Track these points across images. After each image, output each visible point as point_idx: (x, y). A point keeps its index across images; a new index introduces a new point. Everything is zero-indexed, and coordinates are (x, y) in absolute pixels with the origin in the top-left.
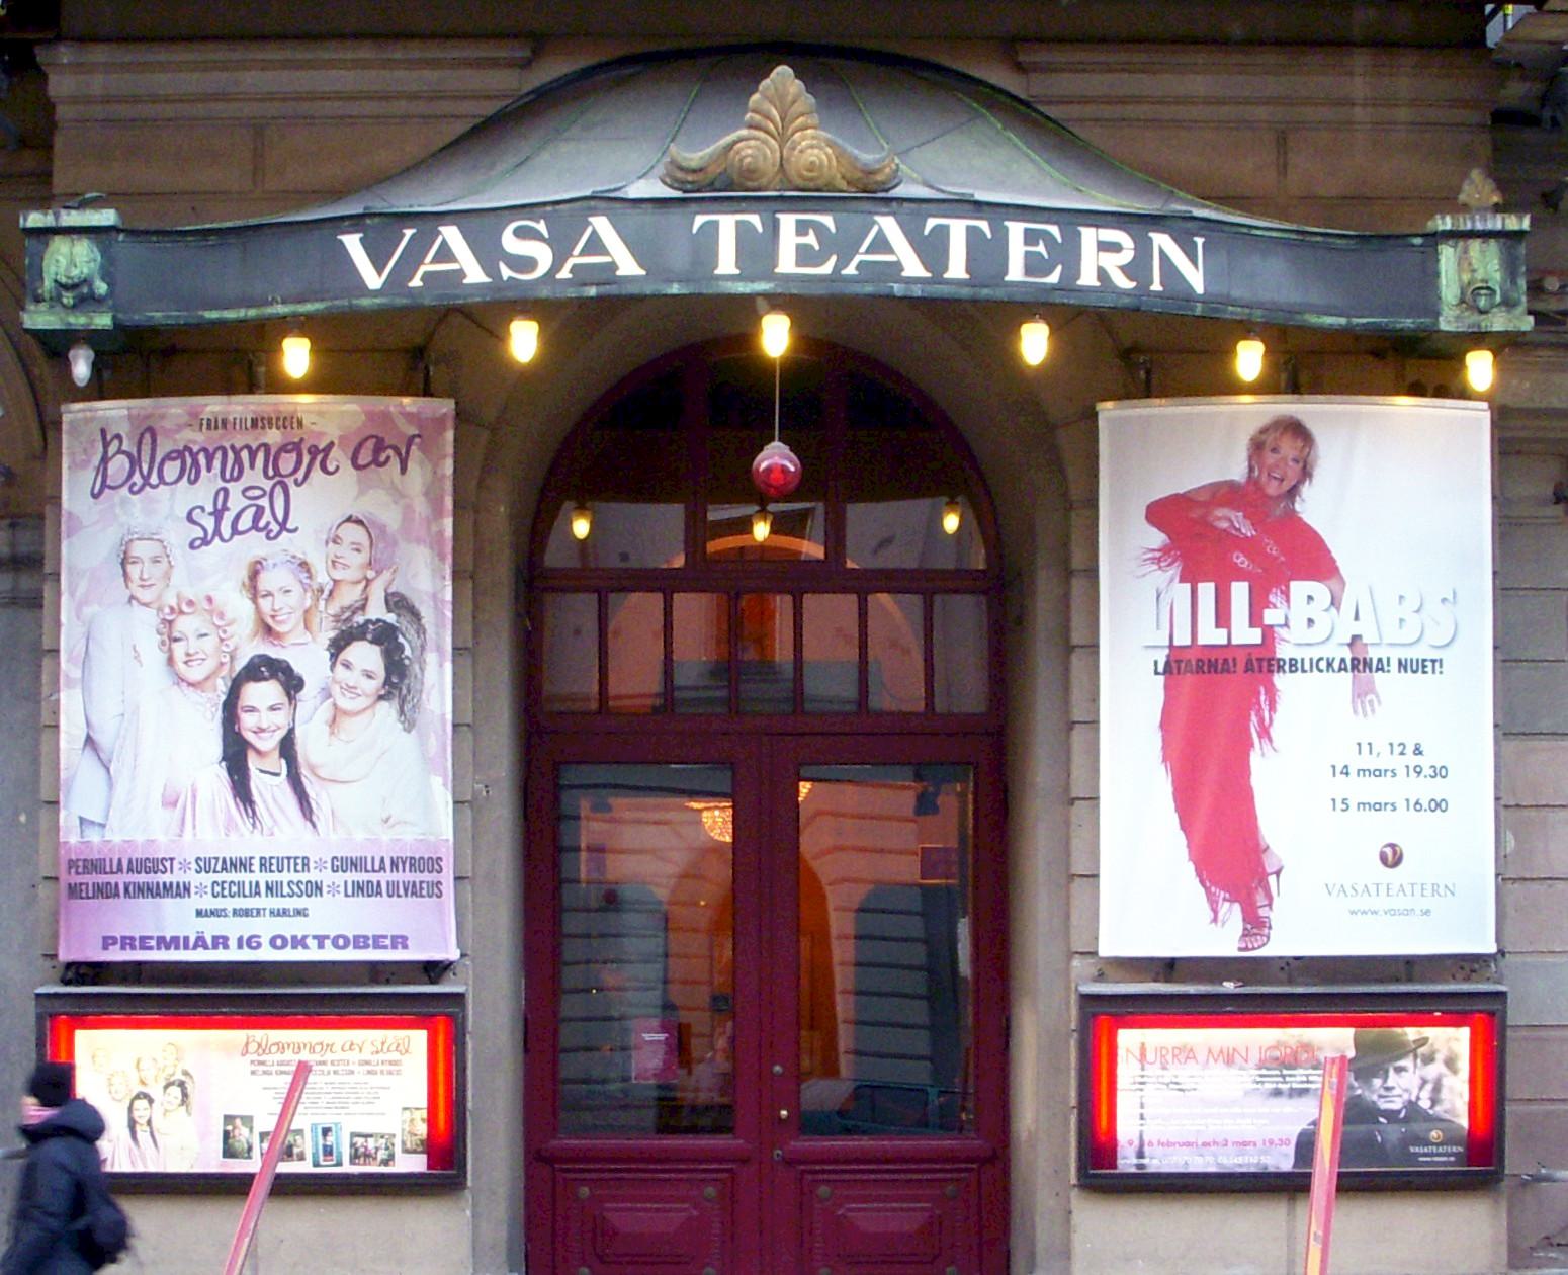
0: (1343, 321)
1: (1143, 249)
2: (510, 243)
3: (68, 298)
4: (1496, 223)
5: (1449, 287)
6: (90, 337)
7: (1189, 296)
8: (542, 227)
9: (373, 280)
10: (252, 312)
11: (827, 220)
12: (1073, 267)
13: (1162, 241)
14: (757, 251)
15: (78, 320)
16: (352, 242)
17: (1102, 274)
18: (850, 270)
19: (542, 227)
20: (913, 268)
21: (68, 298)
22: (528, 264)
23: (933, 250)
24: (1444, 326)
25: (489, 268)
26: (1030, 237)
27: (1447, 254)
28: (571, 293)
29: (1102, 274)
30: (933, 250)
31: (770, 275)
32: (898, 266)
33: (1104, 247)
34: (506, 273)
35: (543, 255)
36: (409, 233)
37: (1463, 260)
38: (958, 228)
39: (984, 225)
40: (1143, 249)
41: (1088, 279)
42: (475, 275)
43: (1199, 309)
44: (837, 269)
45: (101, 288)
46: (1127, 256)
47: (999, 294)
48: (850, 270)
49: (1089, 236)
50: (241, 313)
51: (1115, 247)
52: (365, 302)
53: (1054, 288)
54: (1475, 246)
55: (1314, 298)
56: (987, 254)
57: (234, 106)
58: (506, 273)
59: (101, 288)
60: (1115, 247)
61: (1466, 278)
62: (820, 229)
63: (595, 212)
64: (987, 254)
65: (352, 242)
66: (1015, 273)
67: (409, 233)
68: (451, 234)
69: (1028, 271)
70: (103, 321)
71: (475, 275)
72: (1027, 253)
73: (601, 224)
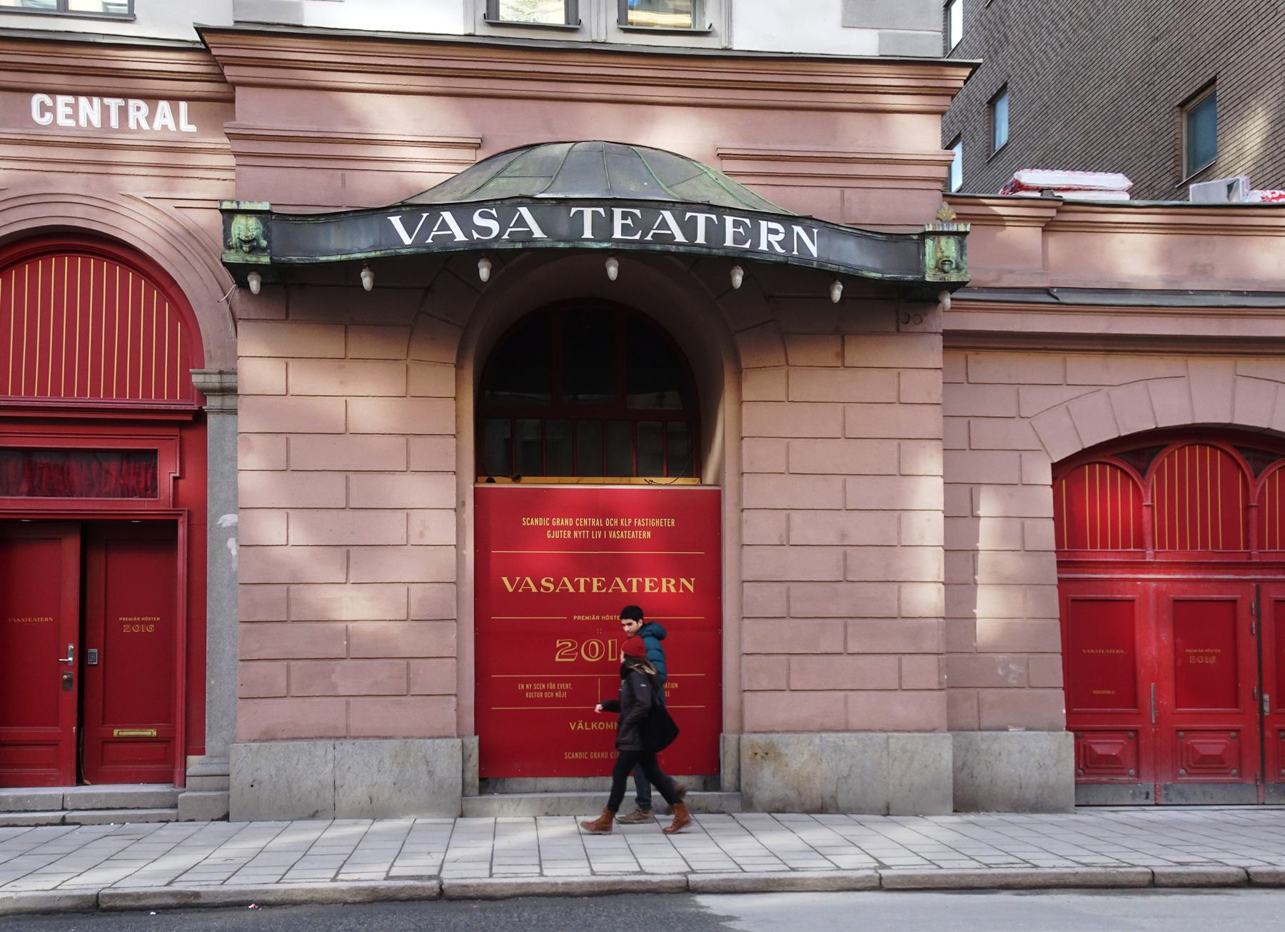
0: (879, 275)
1: (789, 233)
2: (477, 220)
3: (246, 248)
4: (954, 228)
5: (930, 261)
6: (257, 268)
7: (811, 259)
8: (494, 212)
9: (407, 240)
10: (344, 257)
11: (637, 212)
12: (757, 242)
13: (798, 229)
14: (603, 227)
15: (252, 259)
16: (396, 221)
17: (770, 244)
18: (649, 238)
19: (494, 212)
20: (680, 237)
21: (246, 248)
22: (488, 231)
23: (689, 228)
24: (928, 279)
25: (467, 233)
26: (736, 224)
27: (929, 243)
28: (510, 246)
29: (770, 244)
30: (689, 228)
31: (610, 239)
32: (673, 236)
33: (771, 231)
34: (476, 236)
35: (495, 226)
36: (425, 215)
37: (937, 247)
38: (701, 218)
39: (714, 217)
40: (789, 233)
41: (763, 247)
42: (460, 236)
43: (815, 265)
44: (643, 236)
45: (264, 243)
46: (781, 237)
47: (721, 252)
48: (649, 238)
49: (764, 225)
50: (338, 258)
51: (776, 232)
52: (403, 251)
53: (747, 251)
54: (943, 240)
55: (869, 264)
56: (716, 231)
57: (853, 862)
58: (476, 236)
59: (264, 243)
60: (776, 232)
61: (939, 255)
62: (633, 215)
63: (522, 205)
64: (716, 231)
65: (396, 221)
66: (729, 242)
67: (425, 215)
68: (447, 216)
69: (735, 241)
70: (265, 260)
71: (460, 236)
72: (694, 466)
73: (524, 211)
